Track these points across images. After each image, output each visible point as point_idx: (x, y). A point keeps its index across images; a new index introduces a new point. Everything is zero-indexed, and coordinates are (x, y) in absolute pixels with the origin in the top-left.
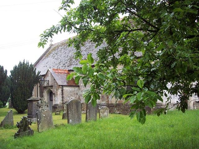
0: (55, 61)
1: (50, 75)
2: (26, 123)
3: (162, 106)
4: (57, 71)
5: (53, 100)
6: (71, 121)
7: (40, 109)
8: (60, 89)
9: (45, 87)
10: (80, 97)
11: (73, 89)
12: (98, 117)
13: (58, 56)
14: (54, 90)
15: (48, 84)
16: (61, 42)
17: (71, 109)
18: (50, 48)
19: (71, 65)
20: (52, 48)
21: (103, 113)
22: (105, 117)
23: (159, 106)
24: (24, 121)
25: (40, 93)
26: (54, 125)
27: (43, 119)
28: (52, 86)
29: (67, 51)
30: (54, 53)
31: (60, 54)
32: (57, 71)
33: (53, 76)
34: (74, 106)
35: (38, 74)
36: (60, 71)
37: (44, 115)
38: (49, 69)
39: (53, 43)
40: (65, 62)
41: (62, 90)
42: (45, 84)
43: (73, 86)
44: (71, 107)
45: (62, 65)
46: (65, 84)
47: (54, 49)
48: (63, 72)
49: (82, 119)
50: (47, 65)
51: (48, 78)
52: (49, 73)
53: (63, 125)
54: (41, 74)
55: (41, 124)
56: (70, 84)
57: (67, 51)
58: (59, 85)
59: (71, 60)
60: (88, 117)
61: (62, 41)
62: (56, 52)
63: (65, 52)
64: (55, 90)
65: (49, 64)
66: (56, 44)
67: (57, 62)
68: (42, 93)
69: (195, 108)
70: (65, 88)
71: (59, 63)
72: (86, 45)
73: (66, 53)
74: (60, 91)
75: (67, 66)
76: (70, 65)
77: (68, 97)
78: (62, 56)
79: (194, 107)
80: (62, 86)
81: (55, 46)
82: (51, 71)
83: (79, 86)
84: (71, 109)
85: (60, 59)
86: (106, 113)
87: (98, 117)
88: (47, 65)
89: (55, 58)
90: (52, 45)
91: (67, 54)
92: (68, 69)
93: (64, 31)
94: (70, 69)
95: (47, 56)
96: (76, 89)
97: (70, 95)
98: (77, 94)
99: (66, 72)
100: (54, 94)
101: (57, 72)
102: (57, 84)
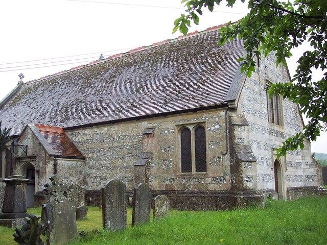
0: (33, 111)
1: (30, 136)
2: (36, 230)
3: (256, 194)
4: (43, 130)
5: (36, 183)
6: (109, 223)
7: (52, 199)
8: (52, 163)
9: (19, 159)
10: (85, 178)
11: (74, 163)
12: (152, 215)
13: (39, 103)
14: (38, 165)
15: (26, 152)
16: (41, 78)
17: (110, 200)
18: (18, 89)
19: (67, 119)
20: (22, 90)
21: (161, 207)
22: (163, 214)
23: (250, 194)
24: (33, 227)
25: (195, 140)
26: (79, 231)
27: (57, 221)
28: (34, 157)
29: (56, 96)
30: (28, 99)
31: (41, 99)
32: (43, 130)
33: (38, 136)
34: (116, 195)
35: (6, 133)
36: (48, 130)
37: (60, 213)
38: (29, 125)
39: (25, 81)
40: (55, 113)
41: (55, 165)
42: (20, 153)
43: (75, 158)
44: (110, 196)
45: (49, 119)
46: (59, 153)
47: (28, 91)
48: (54, 131)
49: (127, 219)
50: (15, 118)
51: (27, 142)
52: (29, 131)
53: (96, 232)
54: (11, 133)
55: (53, 231)
56: (68, 154)
57: (56, 96)
58: (50, 156)
59: (66, 110)
60: (137, 214)
61: (44, 77)
62: (33, 95)
63: (51, 97)
64: (41, 165)
65: (19, 116)
66: (30, 82)
67: (38, 114)
68: (12, 169)
69: (290, 199)
70: (61, 162)
71: (42, 116)
72: (95, 85)
73: (53, 98)
74: (50, 166)
75: (59, 121)
76: (66, 119)
77: (65, 178)
78: (47, 103)
79: (288, 196)
80: (56, 156)
81: (29, 86)
82: (33, 129)
83: (84, 158)
84: (110, 200)
85: (41, 110)
86: (164, 208)
87: (152, 215)
88: (15, 118)
89: (32, 106)
90: (23, 84)
91: (56, 100)
92: (61, 127)
93: (205, 6)
94: (66, 126)
95: (14, 103)
96: (80, 163)
97: (67, 175)
98: (81, 172)
99: (59, 132)
100: (38, 171)
101: (43, 131)
102: (46, 152)
